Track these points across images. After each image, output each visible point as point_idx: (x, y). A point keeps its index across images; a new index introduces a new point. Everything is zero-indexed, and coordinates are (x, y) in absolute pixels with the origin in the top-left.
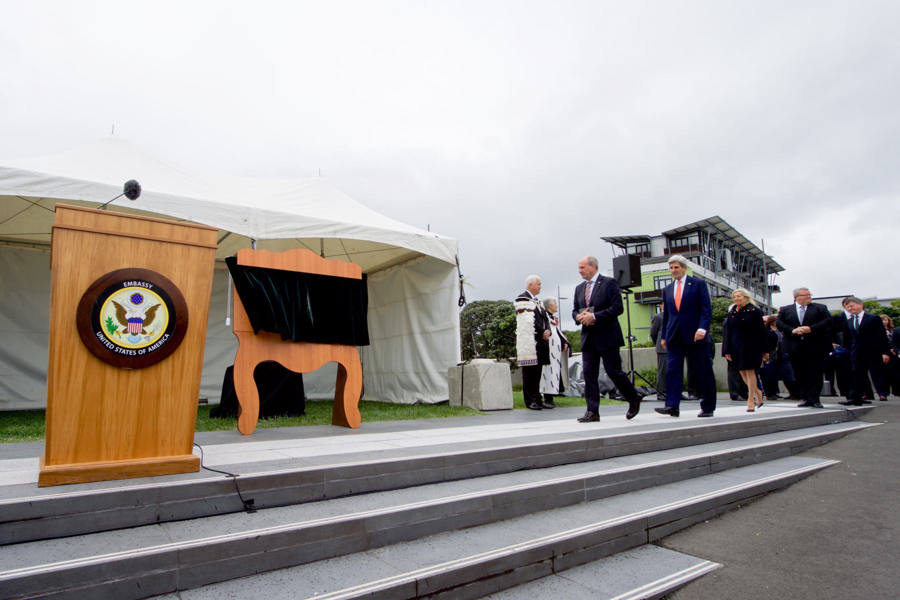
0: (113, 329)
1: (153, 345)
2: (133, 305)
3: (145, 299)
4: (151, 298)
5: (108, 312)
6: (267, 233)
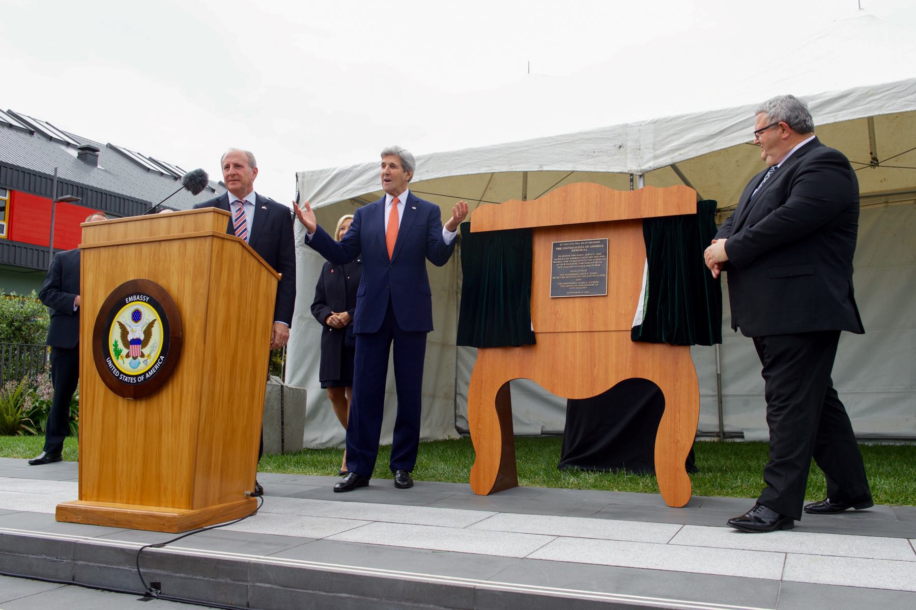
0: (118, 353)
1: (149, 370)
2: (133, 323)
3: (130, 315)
4: (149, 314)
5: (115, 334)
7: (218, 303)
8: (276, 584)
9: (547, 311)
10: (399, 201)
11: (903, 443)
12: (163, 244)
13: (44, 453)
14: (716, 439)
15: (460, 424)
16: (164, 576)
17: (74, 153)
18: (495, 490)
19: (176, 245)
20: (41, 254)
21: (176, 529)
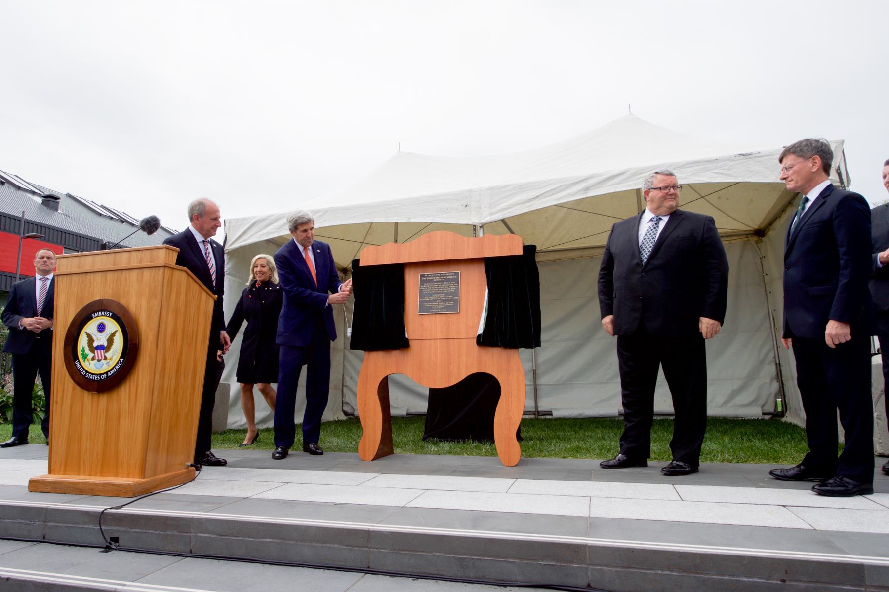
0: (85, 357)
2: (98, 333)
4: (112, 326)
5: (83, 342)
6: (491, 214)
7: (167, 317)
8: (214, 534)
9: (416, 323)
11: (662, 418)
12: (124, 272)
13: (13, 438)
14: (533, 417)
15: (346, 409)
16: (122, 531)
17: (39, 200)
18: (379, 456)
19: (134, 274)
20: (9, 279)
21: (131, 494)
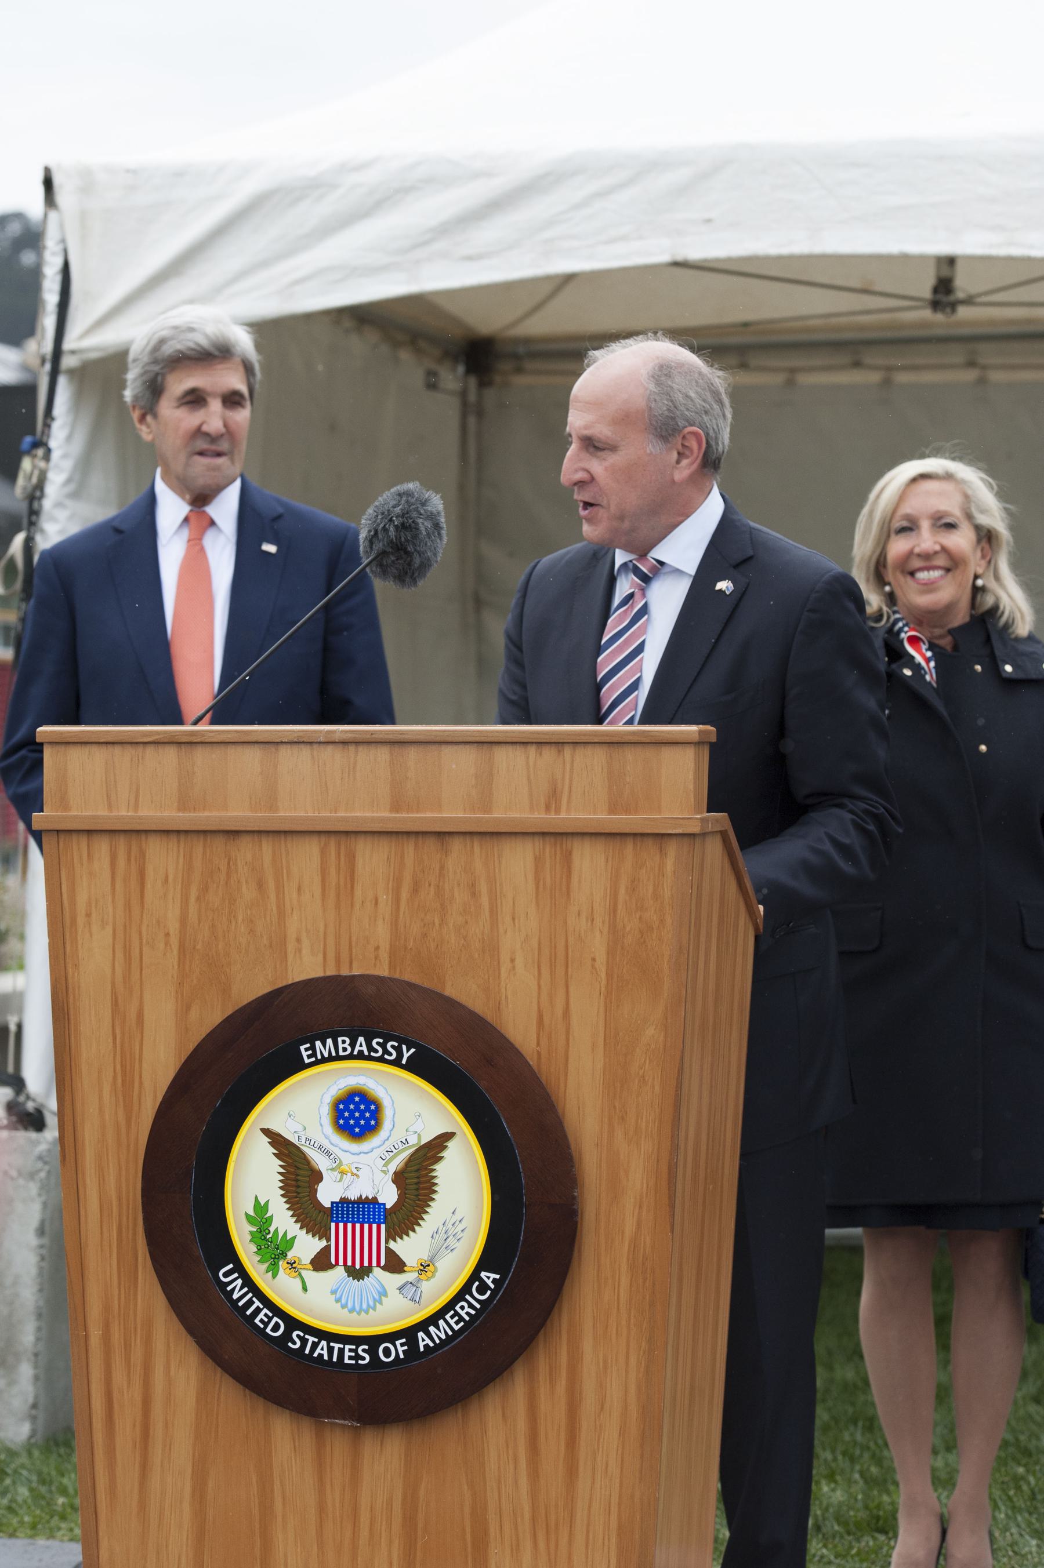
0: (275, 1251)
1: (433, 1320)
2: (341, 1144)
3: (387, 1114)
4: (415, 1109)
5: (252, 1178)
10: (212, 523)
19: (517, 863)
